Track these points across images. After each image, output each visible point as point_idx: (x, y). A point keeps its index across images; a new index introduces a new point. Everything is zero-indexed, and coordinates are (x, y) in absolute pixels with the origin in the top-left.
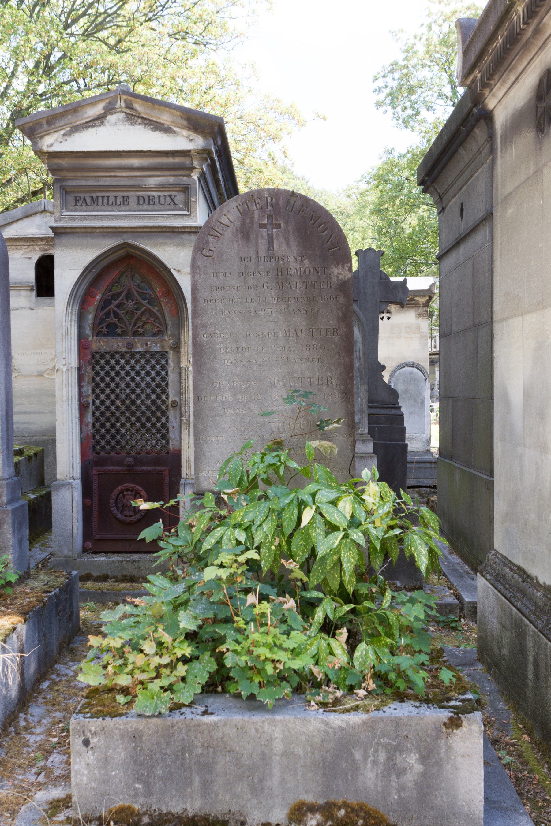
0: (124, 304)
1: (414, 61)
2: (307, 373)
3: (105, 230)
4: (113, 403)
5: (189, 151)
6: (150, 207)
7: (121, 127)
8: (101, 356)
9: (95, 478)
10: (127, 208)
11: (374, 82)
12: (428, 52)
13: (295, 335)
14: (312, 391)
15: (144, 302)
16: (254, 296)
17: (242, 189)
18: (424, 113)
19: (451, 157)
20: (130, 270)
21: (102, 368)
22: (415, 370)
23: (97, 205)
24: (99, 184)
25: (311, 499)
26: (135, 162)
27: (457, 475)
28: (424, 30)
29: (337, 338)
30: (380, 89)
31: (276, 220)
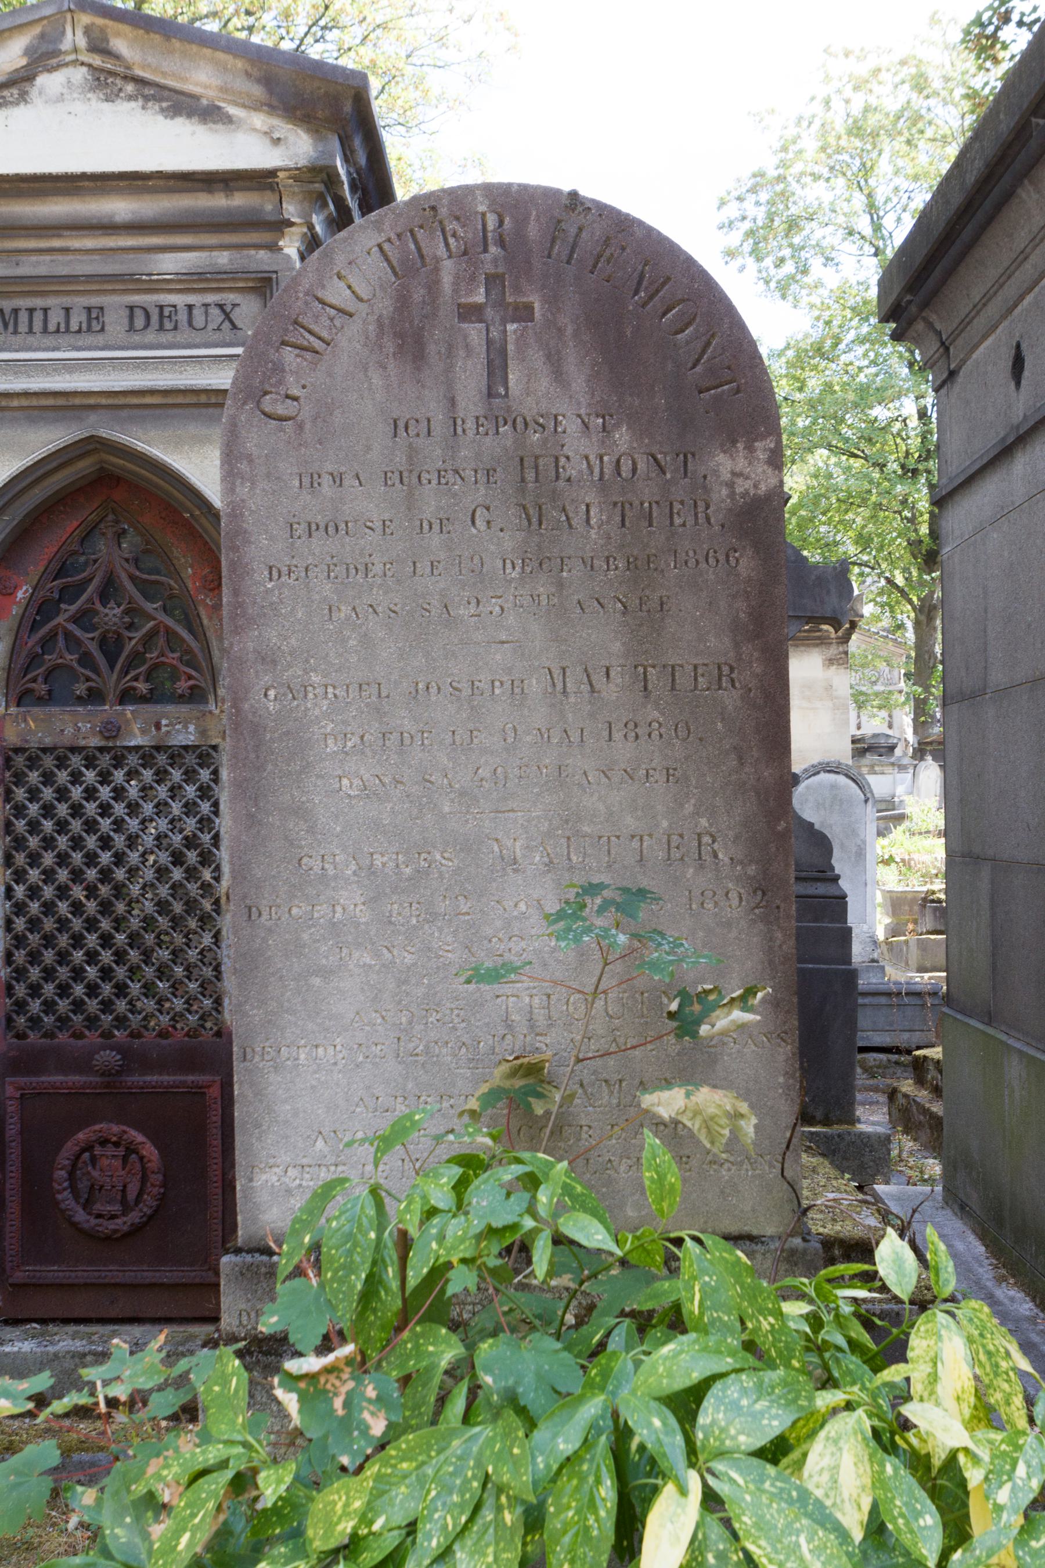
0: (96, 613)
1: (798, 167)
2: (629, 820)
3: (34, 402)
4: (63, 892)
5: (272, 173)
6: (165, 338)
7: (78, 107)
8: (29, 759)
9: (12, 1107)
10: (100, 339)
11: (719, 208)
12: (823, 149)
13: (585, 688)
14: (645, 883)
15: (149, 607)
16: (442, 555)
17: (402, 192)
18: (817, 268)
19: (990, 220)
20: (111, 517)
21: (34, 795)
22: (842, 779)
23: (16, 332)
24: (20, 271)
25: (679, 1439)
26: (120, 207)
27: (1014, 1070)
28: (817, 108)
29: (730, 698)
30: (731, 223)
31: (517, 290)
